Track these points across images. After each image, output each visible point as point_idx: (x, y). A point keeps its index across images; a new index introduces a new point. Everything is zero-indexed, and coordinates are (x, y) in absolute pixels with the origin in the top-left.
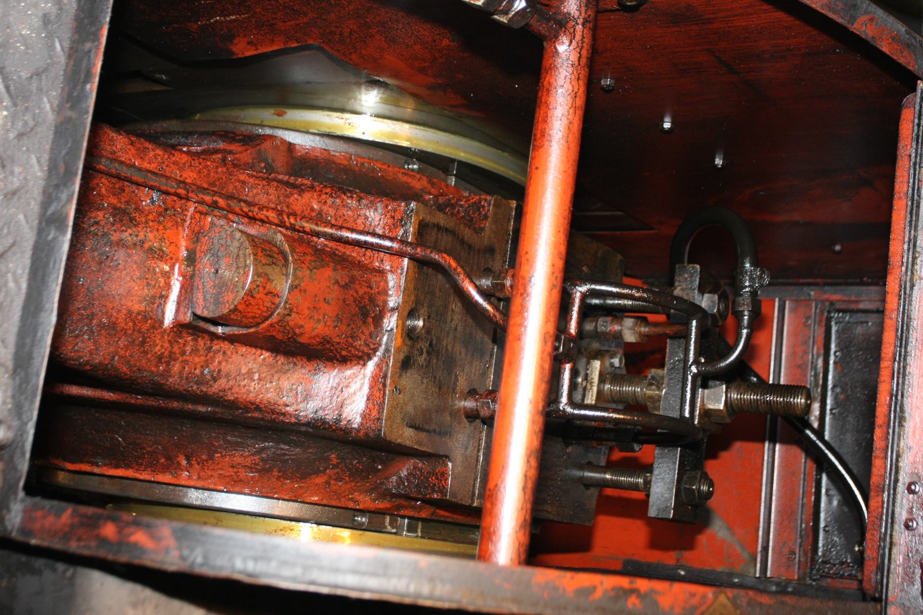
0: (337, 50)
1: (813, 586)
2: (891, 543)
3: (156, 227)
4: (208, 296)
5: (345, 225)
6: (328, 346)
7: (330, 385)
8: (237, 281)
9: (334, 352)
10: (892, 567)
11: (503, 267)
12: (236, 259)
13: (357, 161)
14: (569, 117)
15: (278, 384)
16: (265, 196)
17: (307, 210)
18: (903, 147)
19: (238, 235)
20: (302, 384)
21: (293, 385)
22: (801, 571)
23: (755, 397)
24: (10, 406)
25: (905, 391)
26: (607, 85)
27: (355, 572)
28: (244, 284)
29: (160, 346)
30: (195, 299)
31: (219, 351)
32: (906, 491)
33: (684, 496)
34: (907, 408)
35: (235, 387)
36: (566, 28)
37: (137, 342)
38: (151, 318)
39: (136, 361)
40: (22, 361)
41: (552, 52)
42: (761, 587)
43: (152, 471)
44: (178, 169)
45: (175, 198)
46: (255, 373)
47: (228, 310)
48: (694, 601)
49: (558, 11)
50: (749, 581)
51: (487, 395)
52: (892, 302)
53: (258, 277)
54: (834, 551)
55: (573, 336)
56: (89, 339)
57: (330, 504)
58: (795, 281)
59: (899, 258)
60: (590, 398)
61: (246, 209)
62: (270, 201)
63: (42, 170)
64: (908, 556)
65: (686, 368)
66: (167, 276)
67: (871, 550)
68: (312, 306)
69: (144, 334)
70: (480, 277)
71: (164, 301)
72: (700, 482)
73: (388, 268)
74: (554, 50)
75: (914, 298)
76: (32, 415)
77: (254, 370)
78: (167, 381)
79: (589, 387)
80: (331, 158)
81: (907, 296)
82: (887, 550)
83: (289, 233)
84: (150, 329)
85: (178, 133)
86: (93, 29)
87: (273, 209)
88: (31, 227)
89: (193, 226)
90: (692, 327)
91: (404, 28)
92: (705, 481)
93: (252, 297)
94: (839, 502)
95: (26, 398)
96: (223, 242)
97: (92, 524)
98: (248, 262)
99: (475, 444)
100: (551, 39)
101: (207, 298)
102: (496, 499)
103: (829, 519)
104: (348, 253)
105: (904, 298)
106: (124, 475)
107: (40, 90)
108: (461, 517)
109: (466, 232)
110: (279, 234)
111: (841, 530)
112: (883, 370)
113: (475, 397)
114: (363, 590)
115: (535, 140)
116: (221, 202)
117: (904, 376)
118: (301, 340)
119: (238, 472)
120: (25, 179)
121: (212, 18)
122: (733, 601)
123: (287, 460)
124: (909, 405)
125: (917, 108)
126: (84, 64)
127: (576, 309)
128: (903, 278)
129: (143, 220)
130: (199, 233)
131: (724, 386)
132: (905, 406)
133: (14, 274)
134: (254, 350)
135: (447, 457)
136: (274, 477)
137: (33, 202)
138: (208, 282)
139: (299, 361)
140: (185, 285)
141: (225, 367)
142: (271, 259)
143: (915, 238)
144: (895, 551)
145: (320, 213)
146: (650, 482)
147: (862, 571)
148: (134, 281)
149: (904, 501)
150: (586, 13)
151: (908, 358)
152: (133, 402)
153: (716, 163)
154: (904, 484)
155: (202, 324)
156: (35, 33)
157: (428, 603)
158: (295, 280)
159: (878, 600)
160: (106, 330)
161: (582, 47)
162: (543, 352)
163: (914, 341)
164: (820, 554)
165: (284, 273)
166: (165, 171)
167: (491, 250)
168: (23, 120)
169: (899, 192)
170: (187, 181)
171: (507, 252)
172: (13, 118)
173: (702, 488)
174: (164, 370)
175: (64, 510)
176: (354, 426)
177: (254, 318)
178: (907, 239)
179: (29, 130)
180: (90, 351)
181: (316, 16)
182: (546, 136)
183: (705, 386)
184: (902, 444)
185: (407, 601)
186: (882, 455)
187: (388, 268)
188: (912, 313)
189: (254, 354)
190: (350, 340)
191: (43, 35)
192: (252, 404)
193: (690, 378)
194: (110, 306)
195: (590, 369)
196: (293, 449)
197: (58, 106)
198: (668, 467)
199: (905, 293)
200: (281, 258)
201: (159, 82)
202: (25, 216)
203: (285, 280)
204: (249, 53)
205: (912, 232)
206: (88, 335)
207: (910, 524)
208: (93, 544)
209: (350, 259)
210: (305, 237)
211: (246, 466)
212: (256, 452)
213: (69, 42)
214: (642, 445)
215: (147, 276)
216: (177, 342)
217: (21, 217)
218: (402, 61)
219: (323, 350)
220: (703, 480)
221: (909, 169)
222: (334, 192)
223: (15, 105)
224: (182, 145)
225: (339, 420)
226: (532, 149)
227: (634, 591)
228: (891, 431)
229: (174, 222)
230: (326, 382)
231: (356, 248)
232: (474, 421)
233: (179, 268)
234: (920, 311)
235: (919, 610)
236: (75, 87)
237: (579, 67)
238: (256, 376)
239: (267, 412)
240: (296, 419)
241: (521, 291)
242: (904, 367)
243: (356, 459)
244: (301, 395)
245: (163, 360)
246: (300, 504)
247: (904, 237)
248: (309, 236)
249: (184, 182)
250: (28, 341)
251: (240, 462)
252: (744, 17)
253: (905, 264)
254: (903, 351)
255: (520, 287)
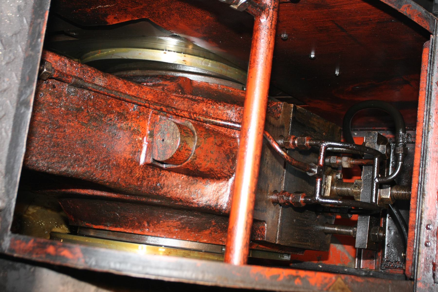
0: (157, 21)
1: (382, 272)
2: (419, 253)
3: (136, 120)
4: (160, 151)
5: (218, 117)
6: (212, 172)
7: (213, 190)
8: (173, 145)
9: (215, 175)
10: (419, 264)
11: (288, 134)
12: (172, 134)
13: (220, 87)
14: (266, 53)
15: (189, 190)
16: (183, 105)
17: (201, 111)
18: (424, 66)
19: (173, 124)
20: (200, 189)
21: (196, 190)
22: (376, 266)
23: (404, 192)
24: (3, 191)
25: (425, 181)
26: (284, 37)
27: (167, 268)
28: (176, 146)
29: (138, 173)
30: (154, 153)
31: (164, 175)
32: (425, 229)
33: (371, 238)
34: (426, 189)
35: (171, 191)
36: (265, 11)
37: (128, 172)
38: (134, 161)
39: (128, 180)
40: (9, 170)
41: (258, 22)
42: (358, 273)
43: (132, 229)
44: (145, 94)
45: (144, 107)
46: (179, 185)
47: (169, 158)
48: (326, 281)
49: (261, 3)
50: (352, 270)
51: (282, 193)
52: (419, 139)
53: (182, 142)
54: (392, 256)
55: (322, 166)
56: (108, 171)
57: (211, 243)
58: (373, 128)
59: (422, 118)
60: (327, 193)
61: (175, 112)
62: (185, 107)
63: (18, 80)
64: (427, 259)
65: (373, 180)
66: (141, 142)
67: (409, 256)
68: (205, 155)
69: (132, 168)
70: (278, 139)
71: (140, 154)
72: (379, 231)
73: (238, 136)
74: (259, 21)
75: (429, 138)
76: (14, 195)
77: (179, 184)
78: (142, 189)
79: (326, 188)
80: (209, 86)
81: (426, 137)
82: (417, 256)
83: (193, 121)
84: (134, 166)
85: (141, 76)
86: (42, 13)
87: (187, 111)
88: (13, 107)
89: (152, 120)
90: (375, 161)
91: (188, 10)
92: (381, 231)
93: (180, 151)
94: (394, 233)
95: (11, 188)
96: (166, 127)
97: (43, 246)
98: (178, 136)
99: (277, 215)
100: (258, 16)
101: (159, 152)
102: (233, 233)
103: (389, 241)
104: (220, 130)
105: (425, 138)
106: (119, 231)
107: (17, 42)
108: (269, 248)
109: (271, 119)
110: (190, 123)
111: (395, 246)
112: (414, 171)
113: (277, 194)
114: (171, 277)
115: (250, 64)
116: (164, 109)
117: (425, 174)
118: (200, 170)
119: (170, 229)
120: (10, 84)
121: (98, 6)
122: (345, 281)
123: (193, 223)
124: (427, 188)
125: (430, 48)
126: (38, 29)
127: (322, 153)
128: (424, 128)
129: (130, 118)
130: (155, 123)
131: (390, 188)
132: (425, 188)
133: (5, 129)
134: (179, 175)
135: (264, 221)
136: (187, 231)
137: (14, 95)
138: (160, 145)
139: (199, 179)
140: (149, 146)
141: (166, 182)
142: (187, 134)
143: (430, 109)
144: (420, 256)
145: (207, 112)
146: (356, 232)
147: (405, 265)
148: (127, 145)
149: (425, 233)
150: (274, 4)
151: (426, 166)
152: (125, 198)
153: (336, 73)
154: (424, 225)
155: (156, 164)
156: (14, 15)
157: (201, 283)
158: (198, 143)
159: (412, 280)
160: (115, 167)
161: (272, 20)
162: (254, 164)
163: (429, 158)
164: (385, 257)
165: (193, 140)
166: (139, 96)
167: (282, 127)
168: (9, 56)
169: (422, 88)
170: (149, 100)
171: (289, 128)
172: (4, 55)
173: (380, 234)
174: (140, 184)
175: (30, 240)
176: (223, 208)
177: (180, 161)
178: (425, 110)
179: (11, 60)
180: (109, 177)
181: (146, 5)
182: (256, 62)
183: (381, 188)
184: (423, 206)
185: (192, 282)
186: (414, 211)
187: (238, 136)
188: (428, 145)
189: (179, 176)
190: (222, 170)
191: (18, 16)
192: (178, 198)
193: (375, 184)
194: (117, 156)
195: (327, 180)
196: (195, 218)
197: (25, 49)
198: (364, 225)
199: (425, 135)
200: (191, 134)
201: (72, 36)
202: (10, 102)
203: (193, 144)
204: (114, 23)
205: (428, 106)
206: (108, 169)
207: (428, 244)
208: (43, 256)
209: (220, 133)
210: (201, 123)
211: (174, 226)
212: (179, 220)
213: (30, 19)
214: (352, 215)
215: (132, 143)
216: (146, 172)
217: (8, 102)
218: (187, 26)
219: (210, 174)
220: (380, 231)
221: (427, 77)
222: (213, 102)
223: (5, 49)
224: (144, 82)
225: (217, 205)
226: (249, 68)
227: (297, 277)
228: (418, 200)
229: (143, 118)
230: (211, 189)
231: (223, 128)
232: (276, 205)
233: (146, 139)
234: (432, 143)
235: (431, 284)
236: (33, 40)
237: (271, 29)
238: (180, 186)
239: (185, 202)
240: (198, 205)
241: (244, 135)
242: (425, 170)
243: (224, 222)
244: (200, 194)
245: (140, 180)
246: (198, 243)
247: (424, 109)
248: (202, 123)
249: (147, 100)
250: (12, 160)
251: (171, 224)
252: (349, 5)
253: (425, 121)
254: (424, 162)
255: (243, 133)
